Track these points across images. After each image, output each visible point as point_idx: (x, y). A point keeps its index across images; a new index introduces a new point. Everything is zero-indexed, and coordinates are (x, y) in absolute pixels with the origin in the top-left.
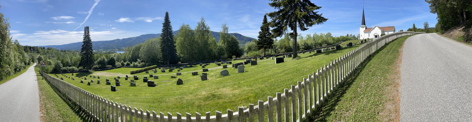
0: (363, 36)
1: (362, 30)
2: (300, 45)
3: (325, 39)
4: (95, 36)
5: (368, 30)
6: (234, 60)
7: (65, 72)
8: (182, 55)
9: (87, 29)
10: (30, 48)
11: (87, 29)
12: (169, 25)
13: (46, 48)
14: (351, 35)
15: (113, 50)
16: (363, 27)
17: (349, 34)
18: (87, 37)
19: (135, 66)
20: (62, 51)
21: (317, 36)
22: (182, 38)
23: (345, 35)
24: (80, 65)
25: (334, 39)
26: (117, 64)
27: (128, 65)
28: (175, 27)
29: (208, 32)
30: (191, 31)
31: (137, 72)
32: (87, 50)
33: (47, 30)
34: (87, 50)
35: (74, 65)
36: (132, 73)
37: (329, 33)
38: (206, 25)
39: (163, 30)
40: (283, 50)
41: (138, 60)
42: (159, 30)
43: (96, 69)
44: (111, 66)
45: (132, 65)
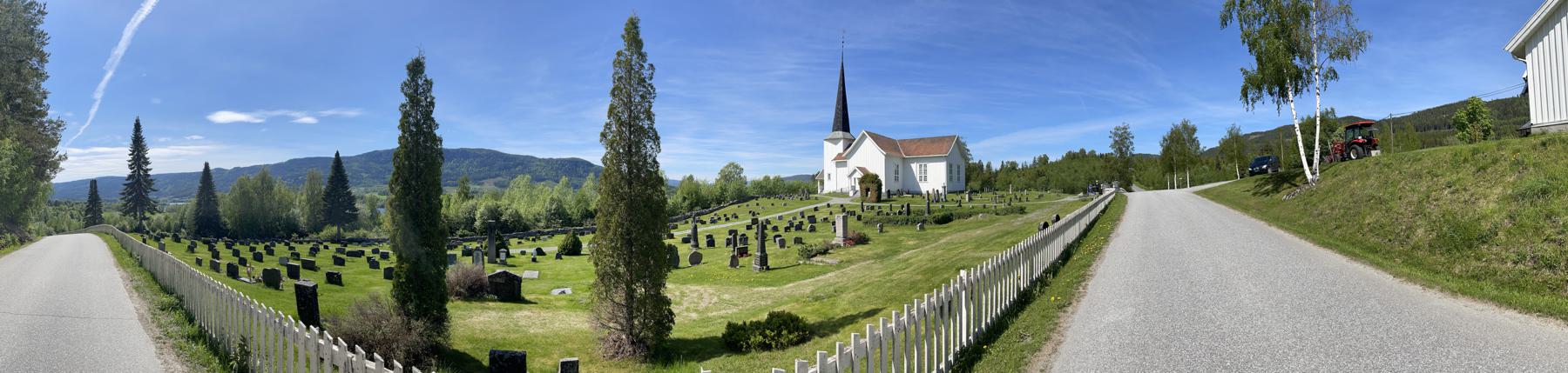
16: (834, 141)
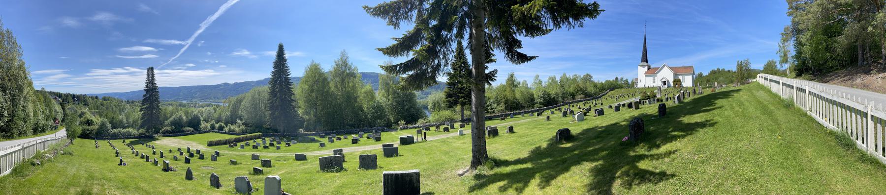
0: (645, 81)
1: (642, 70)
2: (535, 96)
3: (581, 85)
4: (162, 80)
5: (652, 72)
6: (402, 129)
7: (115, 137)
8: (306, 117)
9: (151, 70)
10: (74, 96)
11: (151, 70)
12: (283, 65)
13: (100, 98)
14: (622, 79)
15: (217, 100)
16: (643, 66)
17: (619, 78)
18: (151, 81)
19: (231, 132)
20: (128, 102)
21: (567, 80)
22: (306, 87)
23: (612, 79)
24: (142, 127)
25: (595, 86)
26: (203, 125)
27: (221, 129)
28: (297, 71)
29: (352, 75)
30: (321, 74)
31: (218, 143)
32: (151, 103)
33: (108, 67)
34: (151, 103)
35: (132, 127)
36: (210, 144)
37: (588, 75)
38: (350, 63)
39: (274, 73)
40: (502, 107)
41: (239, 121)
42: (266, 73)
43: (167, 134)
44: (192, 129)
45: (226, 129)
